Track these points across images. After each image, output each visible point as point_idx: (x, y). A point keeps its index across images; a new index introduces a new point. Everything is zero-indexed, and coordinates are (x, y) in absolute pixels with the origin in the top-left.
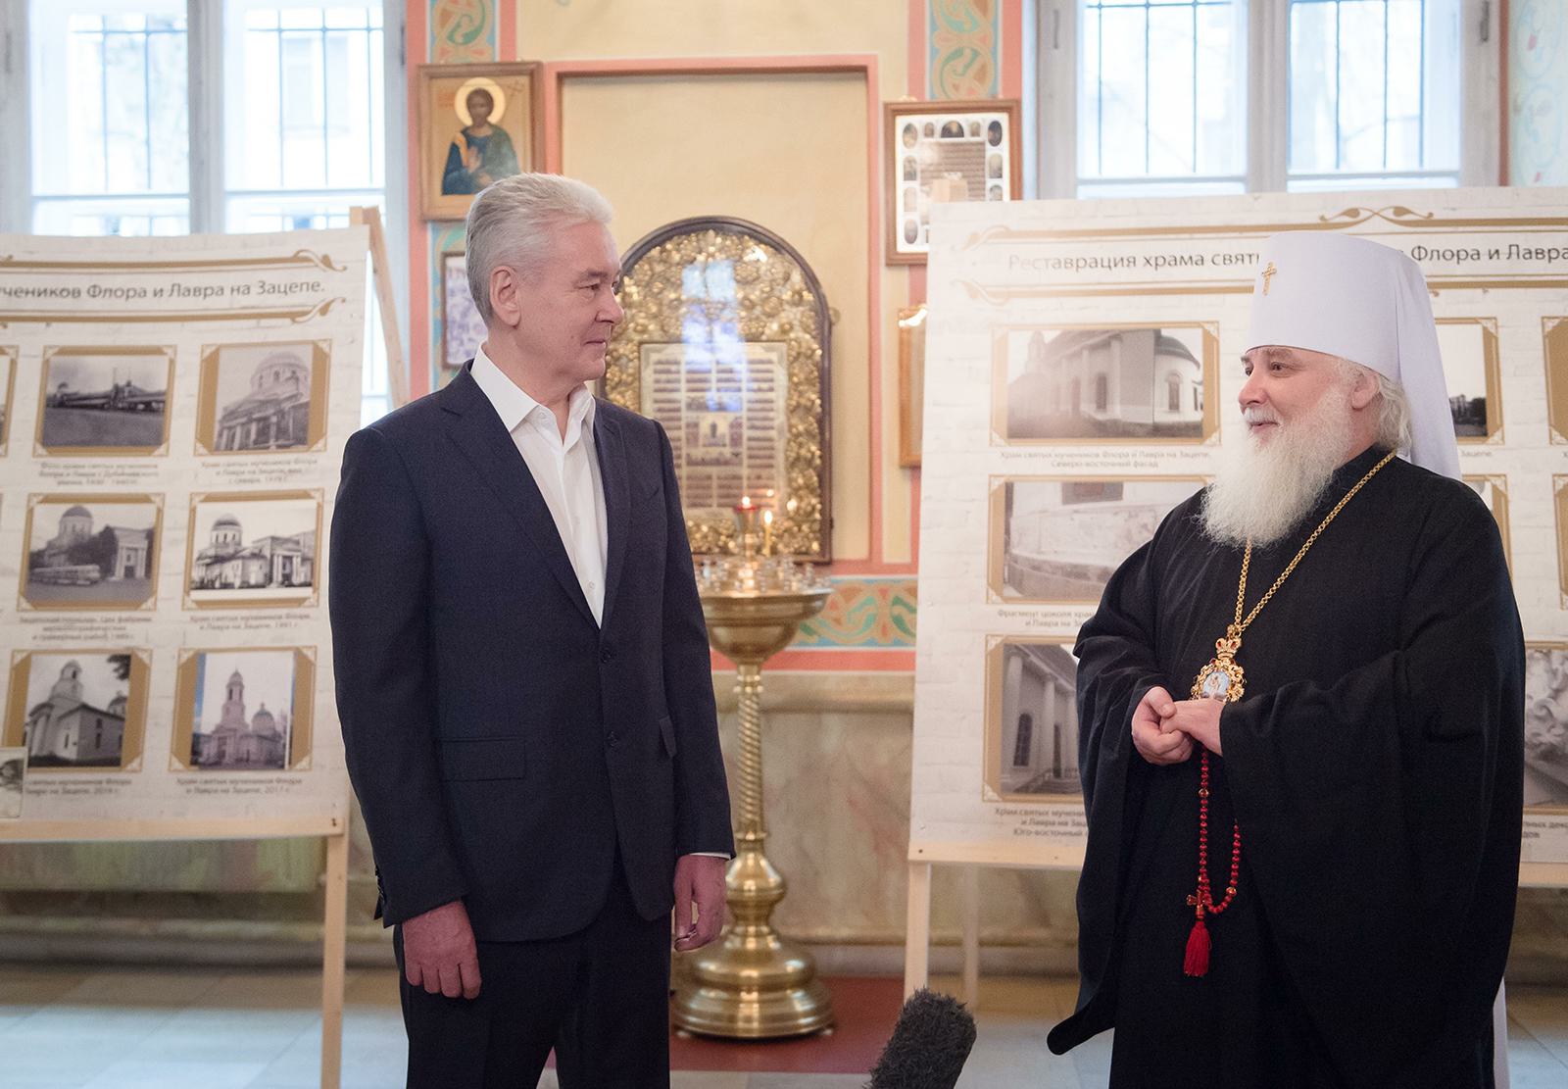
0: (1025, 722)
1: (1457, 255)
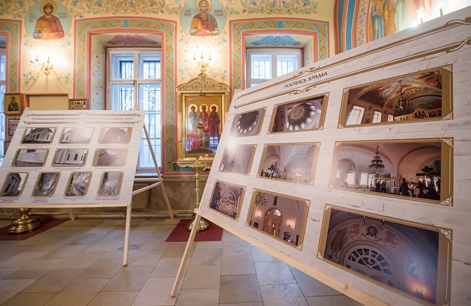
0: (9, 185)
1: (62, 119)
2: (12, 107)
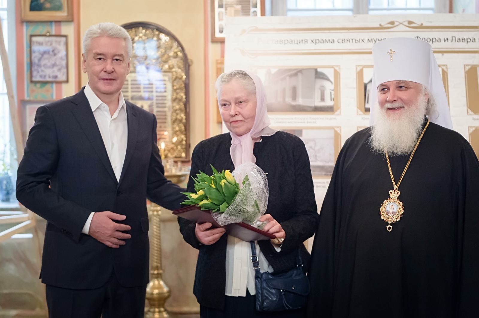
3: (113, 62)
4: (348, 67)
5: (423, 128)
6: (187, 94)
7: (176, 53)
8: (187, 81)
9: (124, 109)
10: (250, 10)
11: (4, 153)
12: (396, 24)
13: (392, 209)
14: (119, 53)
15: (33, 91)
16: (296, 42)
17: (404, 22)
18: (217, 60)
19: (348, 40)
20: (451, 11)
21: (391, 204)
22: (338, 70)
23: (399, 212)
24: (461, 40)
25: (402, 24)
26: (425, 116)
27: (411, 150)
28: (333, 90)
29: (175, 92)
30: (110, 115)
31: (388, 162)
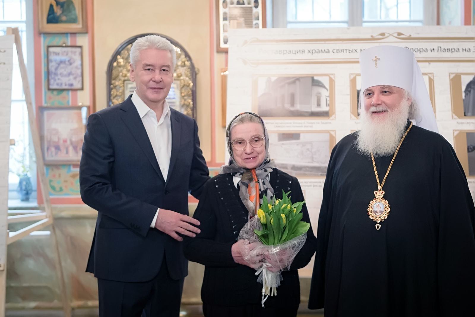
2: (58, 11)
3: (161, 72)
4: (342, 76)
5: (406, 130)
6: (194, 99)
7: (184, 62)
8: (194, 89)
9: (168, 117)
10: (252, 22)
11: (23, 156)
12: (387, 35)
13: (379, 209)
14: (166, 64)
15: (50, 98)
16: (294, 52)
17: (393, 33)
18: (222, 69)
19: (342, 50)
20: (438, 23)
21: (377, 204)
22: (333, 78)
23: (386, 211)
24: (446, 50)
25: (392, 35)
26: (408, 120)
27: (393, 151)
28: (328, 97)
29: (183, 98)
30: (156, 119)
31: (374, 164)
